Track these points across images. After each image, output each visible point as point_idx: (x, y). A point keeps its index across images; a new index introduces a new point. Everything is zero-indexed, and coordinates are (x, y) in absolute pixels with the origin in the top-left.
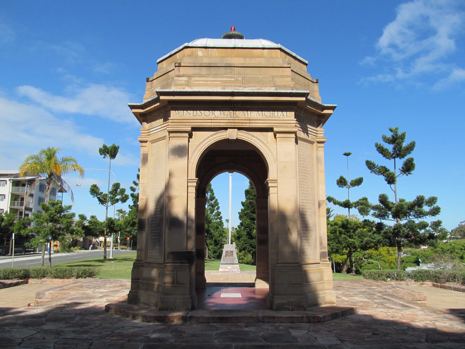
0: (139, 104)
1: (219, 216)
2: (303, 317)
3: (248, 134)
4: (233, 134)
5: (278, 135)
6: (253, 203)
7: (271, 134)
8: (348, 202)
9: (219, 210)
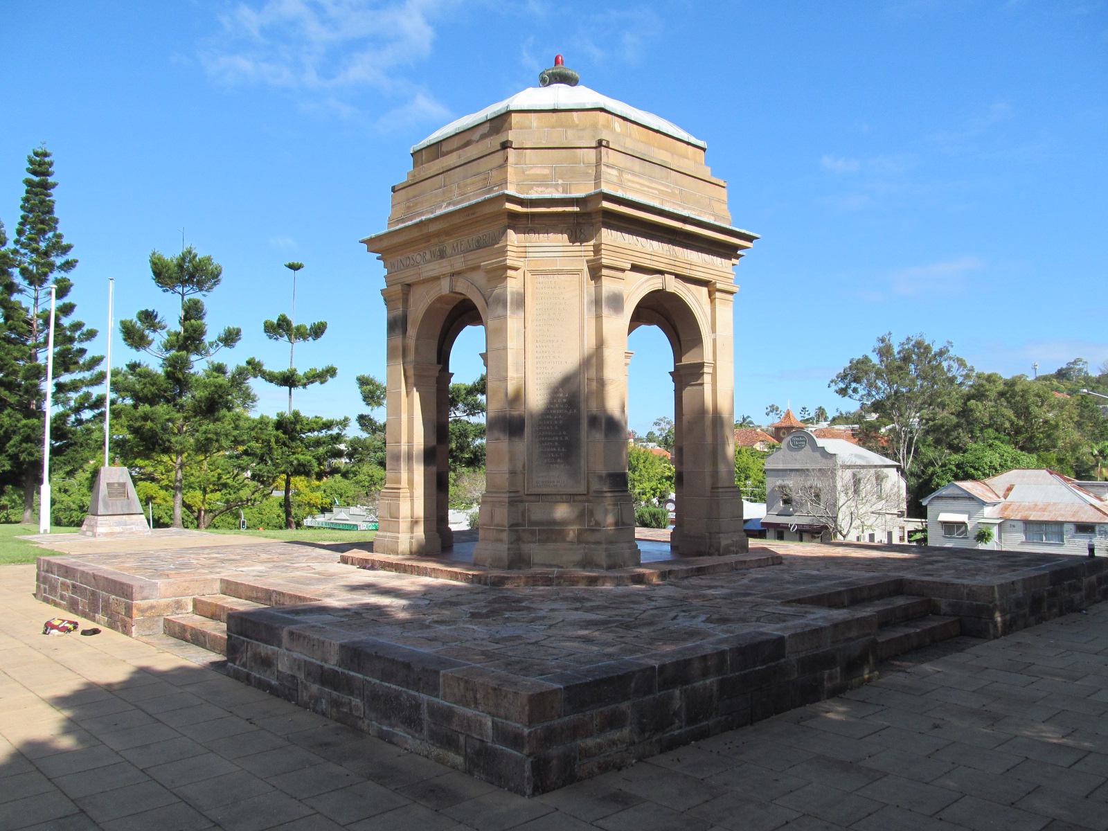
0: (522, 196)
2: (768, 558)
3: (685, 287)
4: (673, 286)
5: (718, 295)
7: (705, 290)
8: (293, 375)
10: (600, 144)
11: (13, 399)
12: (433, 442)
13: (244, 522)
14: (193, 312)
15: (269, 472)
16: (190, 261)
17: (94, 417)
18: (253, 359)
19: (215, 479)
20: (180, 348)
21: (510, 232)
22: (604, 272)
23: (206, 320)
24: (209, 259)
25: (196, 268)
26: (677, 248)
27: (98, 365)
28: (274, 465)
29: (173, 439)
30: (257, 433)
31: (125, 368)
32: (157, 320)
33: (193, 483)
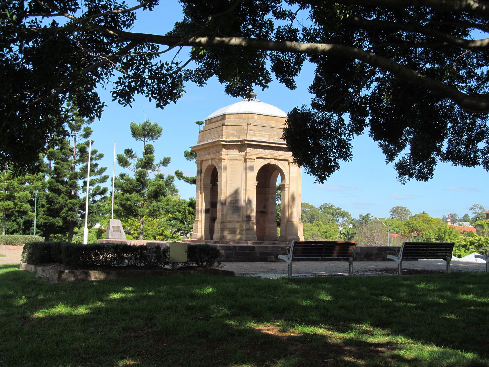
4: (273, 162)
6: (60, 170)
7: (287, 162)
10: (248, 125)
11: (64, 189)
12: (209, 207)
14: (149, 150)
15: (185, 228)
16: (148, 126)
17: (101, 199)
18: (178, 171)
20: (143, 167)
21: (223, 149)
22: (247, 160)
23: (155, 154)
24: (156, 124)
25: (150, 130)
26: (275, 151)
27: (104, 172)
29: (139, 210)
31: (119, 176)
32: (133, 154)
33: (149, 234)
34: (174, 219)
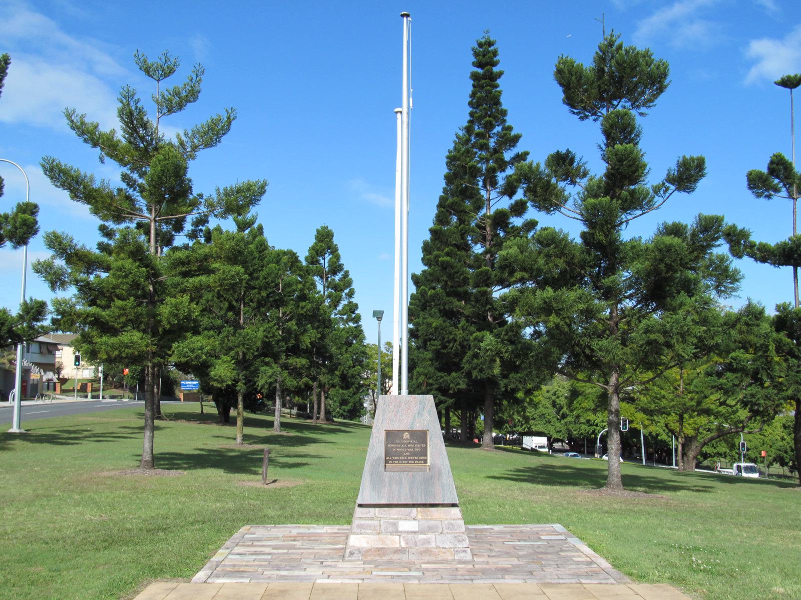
1: (353, 313)
6: (452, 267)
9: (352, 300)
13: (743, 444)
19: (694, 403)
28: (775, 387)
30: (741, 332)
33: (664, 408)
34: (729, 368)
